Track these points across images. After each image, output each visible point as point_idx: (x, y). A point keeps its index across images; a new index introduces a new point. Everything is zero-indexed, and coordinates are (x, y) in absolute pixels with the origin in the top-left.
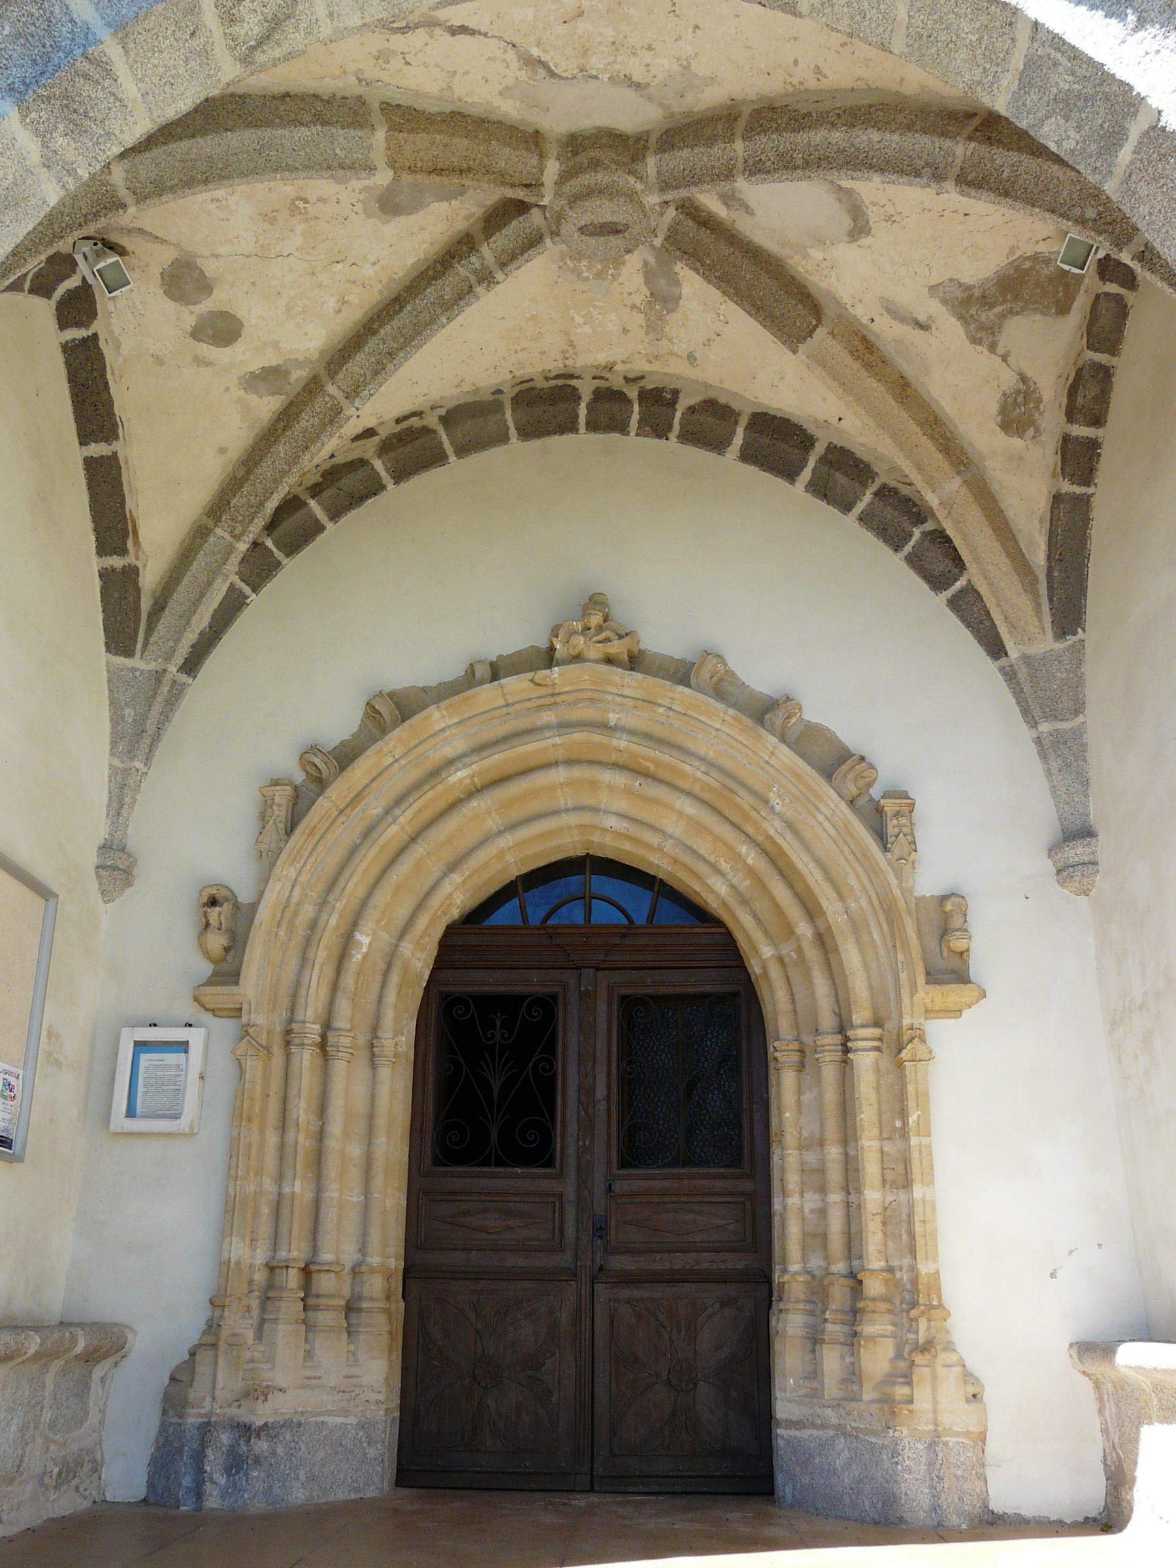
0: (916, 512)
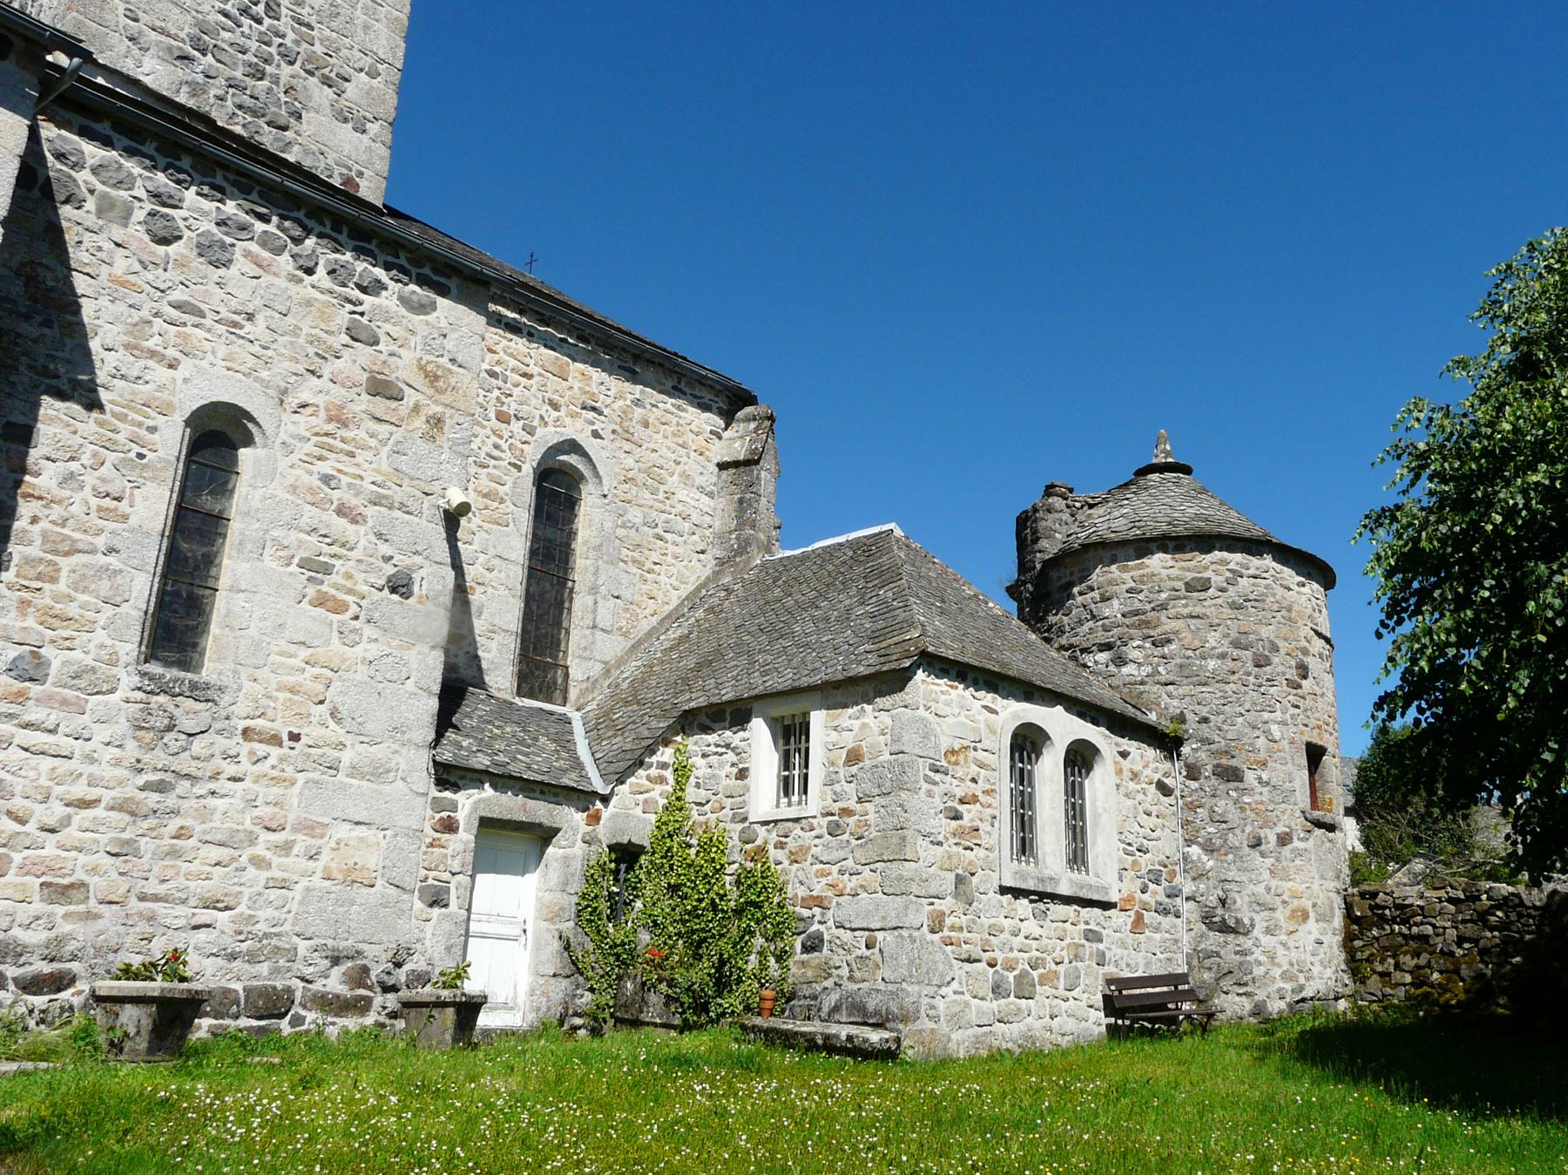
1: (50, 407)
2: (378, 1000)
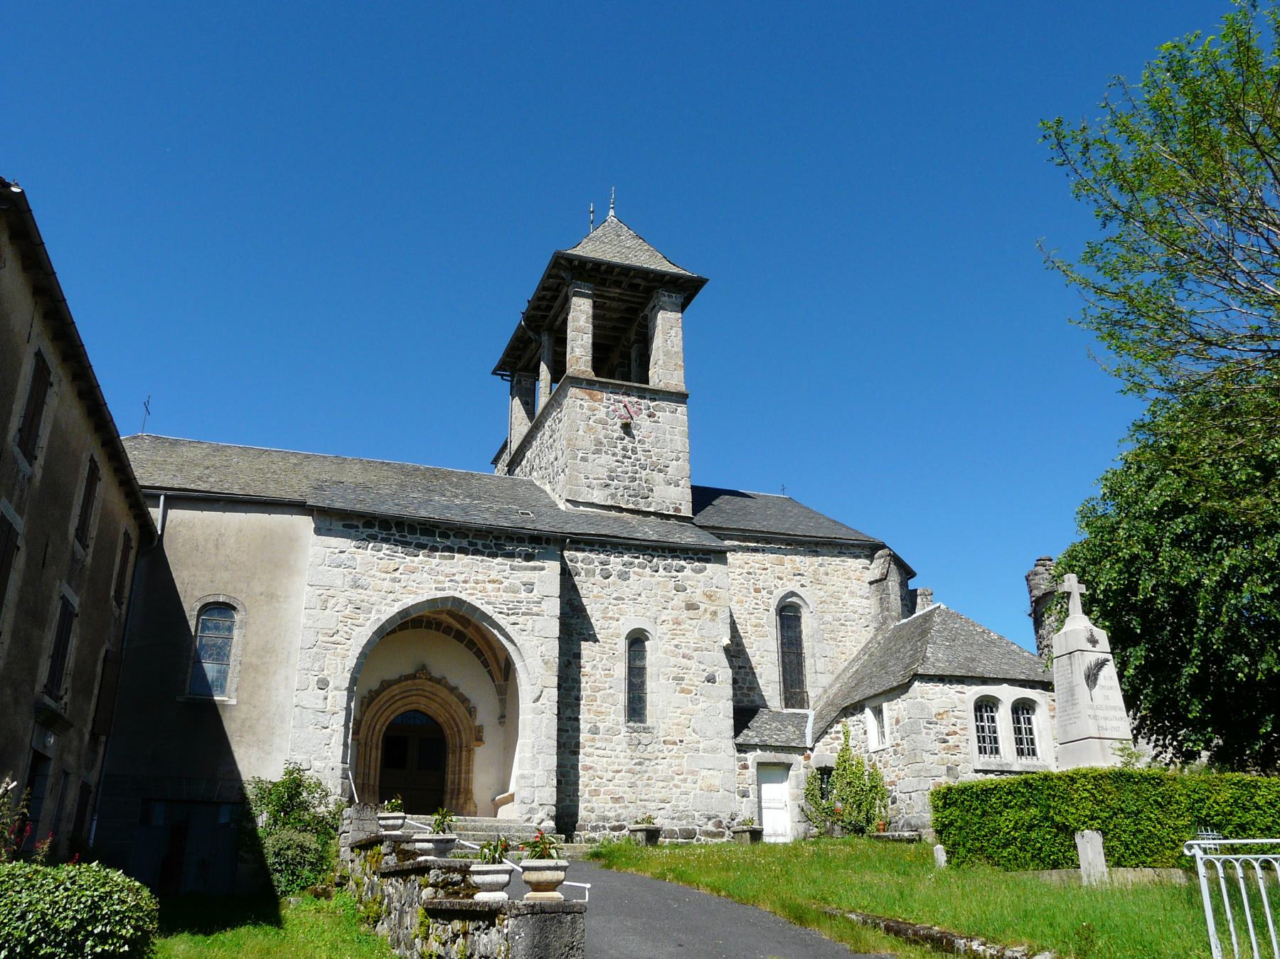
0: (475, 644)
1: (584, 645)
2: (727, 832)
